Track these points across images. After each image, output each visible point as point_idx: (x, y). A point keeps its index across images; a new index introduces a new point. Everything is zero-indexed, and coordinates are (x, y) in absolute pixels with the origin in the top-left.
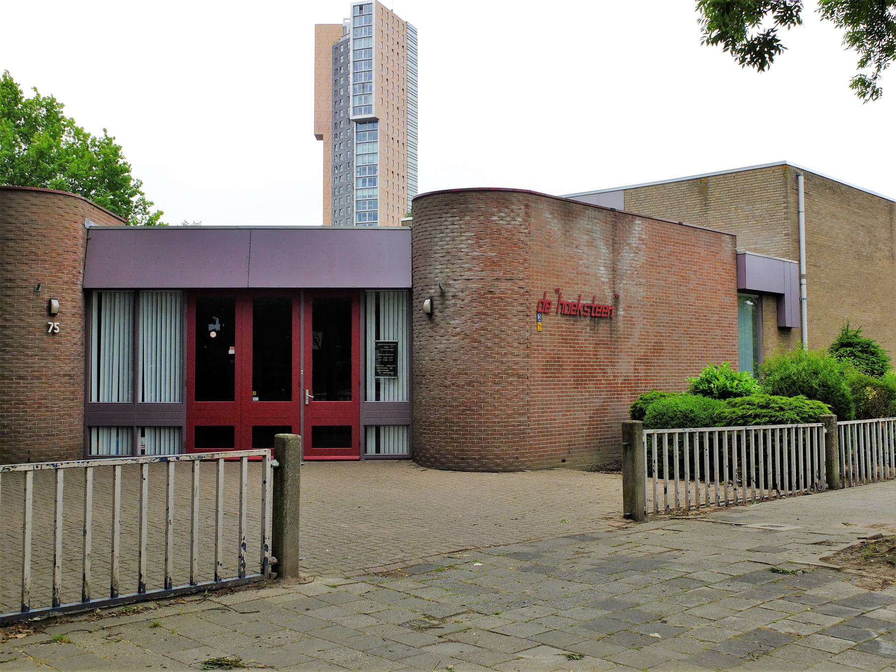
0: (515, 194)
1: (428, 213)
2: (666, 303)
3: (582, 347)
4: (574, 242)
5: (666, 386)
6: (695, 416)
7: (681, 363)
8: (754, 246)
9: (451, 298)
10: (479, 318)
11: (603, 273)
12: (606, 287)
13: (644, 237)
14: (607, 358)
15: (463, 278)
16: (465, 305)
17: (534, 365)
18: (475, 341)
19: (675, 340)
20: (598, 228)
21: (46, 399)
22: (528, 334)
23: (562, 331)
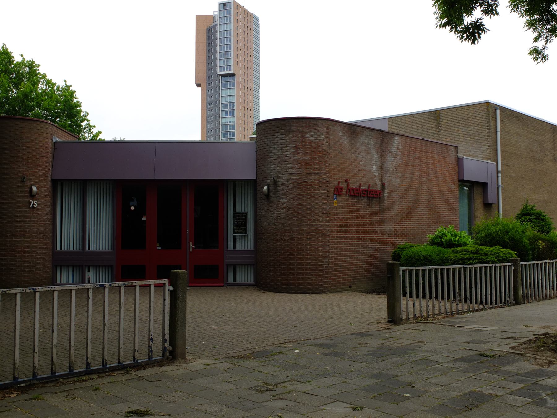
0: (320, 121)
1: (266, 132)
2: (414, 189)
3: (362, 216)
4: (357, 151)
7: (423, 226)
8: (469, 153)
9: (280, 185)
13: (400, 147)
14: (378, 223)
15: (288, 173)
16: (289, 190)
17: (332, 227)
18: (295, 212)
20: (371, 142)
21: (29, 248)
22: (328, 208)
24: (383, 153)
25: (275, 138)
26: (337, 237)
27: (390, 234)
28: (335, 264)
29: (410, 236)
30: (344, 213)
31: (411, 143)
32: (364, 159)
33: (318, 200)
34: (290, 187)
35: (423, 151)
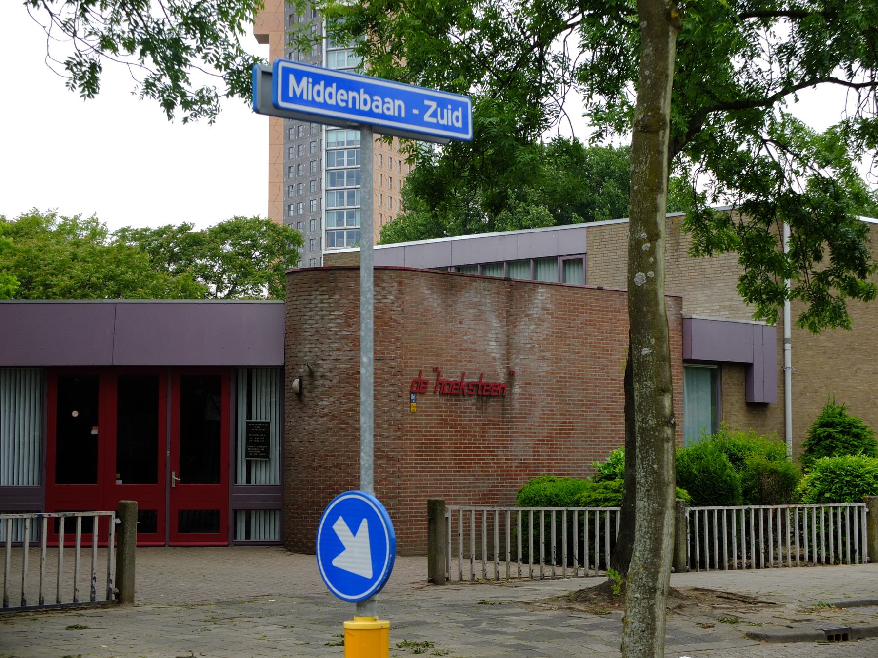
0: (387, 272)
1: (299, 290)
2: (578, 378)
3: (466, 428)
4: (458, 317)
5: (578, 471)
6: (559, 500)
7: (599, 445)
8: (729, 303)
9: (319, 378)
10: (347, 399)
11: (494, 348)
12: (498, 363)
13: (549, 306)
14: (498, 440)
15: (332, 358)
16: (333, 386)
17: (407, 447)
18: (343, 422)
19: (590, 419)
20: (488, 301)
22: (399, 416)
23: (441, 412)
24: (511, 319)
25: (311, 300)
26: (415, 463)
27: (524, 459)
28: (410, 509)
29: (567, 463)
30: (430, 423)
31: (574, 297)
32: (471, 331)
33: (382, 403)
34: (335, 382)
35: (599, 310)
